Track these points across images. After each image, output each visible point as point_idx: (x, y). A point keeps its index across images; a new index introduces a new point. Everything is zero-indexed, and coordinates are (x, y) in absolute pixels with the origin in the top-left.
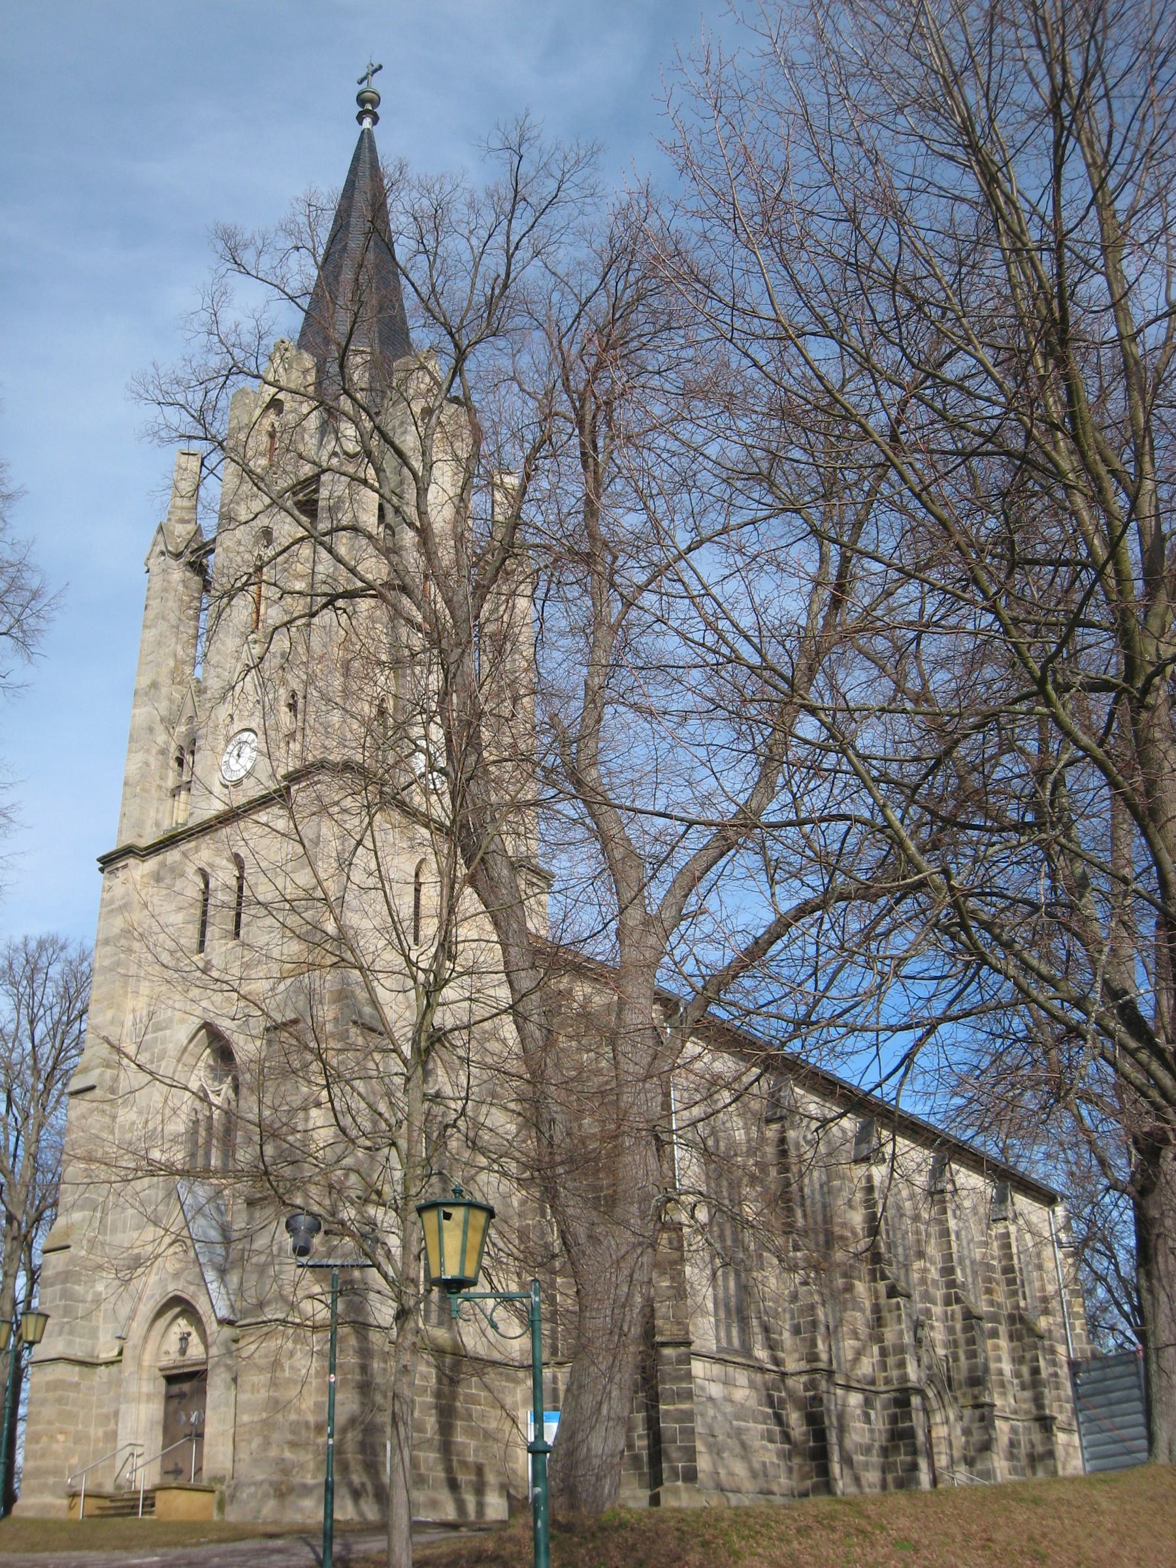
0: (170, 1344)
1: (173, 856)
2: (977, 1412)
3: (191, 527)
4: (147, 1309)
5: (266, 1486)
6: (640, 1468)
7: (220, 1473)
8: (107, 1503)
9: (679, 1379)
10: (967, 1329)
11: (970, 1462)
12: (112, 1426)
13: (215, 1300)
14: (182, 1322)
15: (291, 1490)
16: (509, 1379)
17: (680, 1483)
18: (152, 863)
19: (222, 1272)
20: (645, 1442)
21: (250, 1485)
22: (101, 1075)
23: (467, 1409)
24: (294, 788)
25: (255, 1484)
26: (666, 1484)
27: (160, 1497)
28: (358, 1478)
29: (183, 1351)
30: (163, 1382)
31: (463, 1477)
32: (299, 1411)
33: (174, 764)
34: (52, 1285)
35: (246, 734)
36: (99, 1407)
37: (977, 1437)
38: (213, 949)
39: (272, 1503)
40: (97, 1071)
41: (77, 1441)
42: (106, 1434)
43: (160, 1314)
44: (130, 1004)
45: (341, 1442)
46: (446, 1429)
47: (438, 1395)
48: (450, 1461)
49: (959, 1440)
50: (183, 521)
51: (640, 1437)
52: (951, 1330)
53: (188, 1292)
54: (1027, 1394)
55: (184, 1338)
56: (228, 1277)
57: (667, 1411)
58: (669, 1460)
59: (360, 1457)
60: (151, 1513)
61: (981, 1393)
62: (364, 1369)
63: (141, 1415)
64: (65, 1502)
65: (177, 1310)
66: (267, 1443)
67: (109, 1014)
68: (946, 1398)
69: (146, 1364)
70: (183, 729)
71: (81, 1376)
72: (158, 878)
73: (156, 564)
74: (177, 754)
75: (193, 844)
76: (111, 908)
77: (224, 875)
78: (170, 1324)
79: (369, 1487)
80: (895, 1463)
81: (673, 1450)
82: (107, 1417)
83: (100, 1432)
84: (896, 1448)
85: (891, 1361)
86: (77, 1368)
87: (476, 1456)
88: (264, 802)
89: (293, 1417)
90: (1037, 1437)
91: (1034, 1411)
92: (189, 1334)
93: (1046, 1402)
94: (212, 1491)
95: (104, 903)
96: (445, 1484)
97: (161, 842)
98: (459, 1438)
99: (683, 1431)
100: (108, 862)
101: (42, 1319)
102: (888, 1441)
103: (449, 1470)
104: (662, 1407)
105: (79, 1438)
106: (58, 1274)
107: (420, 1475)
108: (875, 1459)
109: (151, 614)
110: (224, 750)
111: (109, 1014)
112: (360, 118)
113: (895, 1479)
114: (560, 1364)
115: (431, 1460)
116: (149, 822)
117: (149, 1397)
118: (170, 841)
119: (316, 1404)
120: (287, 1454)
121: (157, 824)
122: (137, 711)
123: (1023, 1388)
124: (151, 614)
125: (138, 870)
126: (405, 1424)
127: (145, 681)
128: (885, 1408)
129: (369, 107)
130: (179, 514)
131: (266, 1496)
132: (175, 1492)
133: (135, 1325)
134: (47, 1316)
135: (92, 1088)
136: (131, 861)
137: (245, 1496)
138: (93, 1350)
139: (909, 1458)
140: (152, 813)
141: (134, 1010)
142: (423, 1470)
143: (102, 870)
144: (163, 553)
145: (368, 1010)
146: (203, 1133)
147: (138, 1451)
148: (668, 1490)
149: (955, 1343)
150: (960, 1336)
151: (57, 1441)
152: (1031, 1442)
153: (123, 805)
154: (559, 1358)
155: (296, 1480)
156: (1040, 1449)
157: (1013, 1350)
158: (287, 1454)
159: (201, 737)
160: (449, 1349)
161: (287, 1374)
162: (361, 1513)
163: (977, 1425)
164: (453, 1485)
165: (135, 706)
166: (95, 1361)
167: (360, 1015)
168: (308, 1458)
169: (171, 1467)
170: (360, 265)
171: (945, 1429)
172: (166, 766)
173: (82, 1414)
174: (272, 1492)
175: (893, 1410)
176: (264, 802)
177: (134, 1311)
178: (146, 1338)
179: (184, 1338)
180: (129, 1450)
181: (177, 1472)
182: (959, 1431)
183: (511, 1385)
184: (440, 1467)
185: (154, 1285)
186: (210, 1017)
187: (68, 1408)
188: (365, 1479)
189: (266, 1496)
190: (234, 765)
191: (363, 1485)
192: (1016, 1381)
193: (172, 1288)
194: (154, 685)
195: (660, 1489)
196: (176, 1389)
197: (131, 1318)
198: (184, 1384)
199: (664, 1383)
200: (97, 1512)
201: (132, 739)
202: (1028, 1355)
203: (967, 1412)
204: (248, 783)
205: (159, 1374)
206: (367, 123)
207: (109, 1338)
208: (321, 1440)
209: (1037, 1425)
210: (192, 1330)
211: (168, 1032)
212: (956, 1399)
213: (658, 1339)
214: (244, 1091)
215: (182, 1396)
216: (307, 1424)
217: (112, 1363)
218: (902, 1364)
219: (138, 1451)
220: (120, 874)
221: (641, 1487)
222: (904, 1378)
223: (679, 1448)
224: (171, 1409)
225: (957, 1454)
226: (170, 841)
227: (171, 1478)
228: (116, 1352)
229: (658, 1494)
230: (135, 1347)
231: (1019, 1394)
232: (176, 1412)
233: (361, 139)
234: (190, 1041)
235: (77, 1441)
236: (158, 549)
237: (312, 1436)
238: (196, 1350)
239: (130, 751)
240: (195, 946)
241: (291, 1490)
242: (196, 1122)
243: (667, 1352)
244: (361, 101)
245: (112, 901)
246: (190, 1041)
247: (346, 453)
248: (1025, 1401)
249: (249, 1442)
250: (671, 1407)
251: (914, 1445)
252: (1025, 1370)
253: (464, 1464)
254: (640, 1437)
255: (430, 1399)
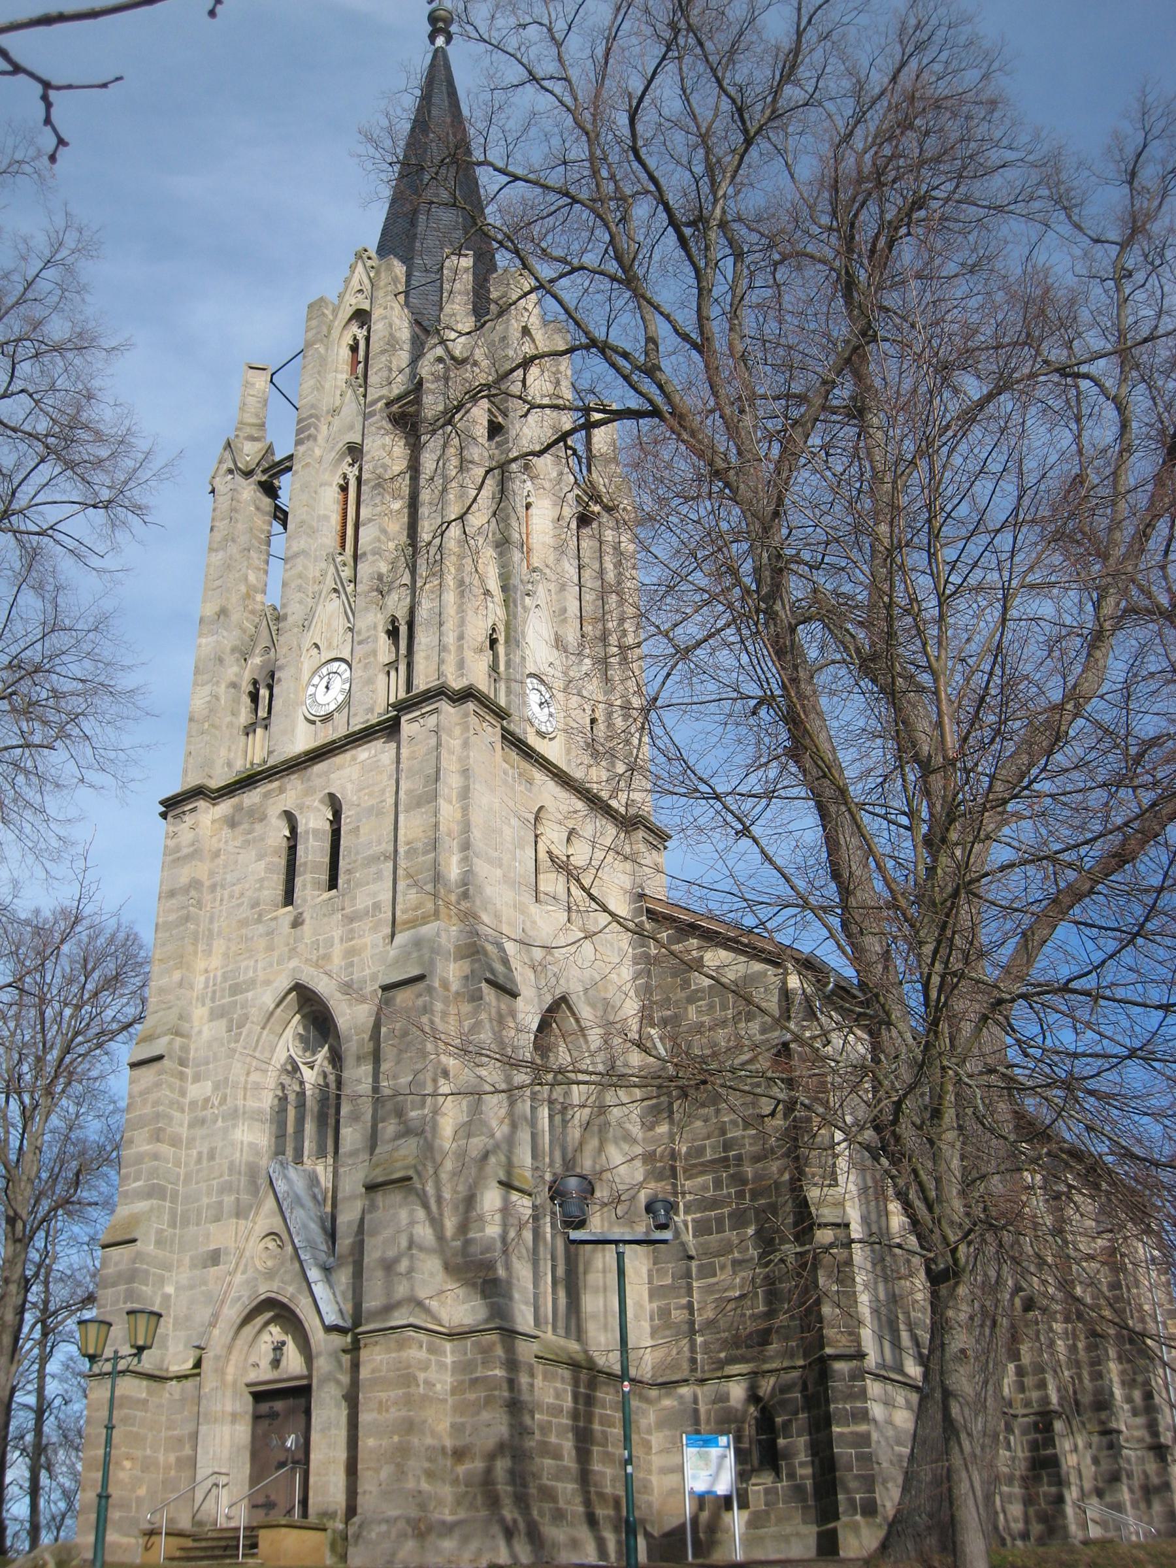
0: (261, 1356)
1: (251, 798)
2: (1105, 1440)
3: (258, 446)
4: (232, 1313)
5: (401, 1524)
6: (804, 1500)
7: (331, 1509)
8: (189, 1543)
9: (850, 1397)
10: (1090, 1348)
11: (1100, 1493)
12: (187, 1451)
13: (325, 1302)
14: (275, 1329)
15: (430, 1529)
16: (647, 1400)
17: (858, 1517)
18: (225, 807)
19: (327, 1270)
20: (808, 1471)
21: (379, 1523)
22: (171, 1042)
23: (603, 1432)
24: (403, 719)
25: (387, 1521)
26: (844, 1519)
27: (264, 1536)
28: (509, 1513)
29: (276, 1363)
30: (250, 1399)
31: (602, 1512)
32: (433, 1434)
33: (247, 700)
34: (114, 1285)
35: (336, 664)
36: (168, 1428)
37: (1105, 1465)
38: (305, 901)
39: (410, 1544)
40: (165, 1039)
41: (145, 1468)
42: (178, 1460)
43: (247, 1319)
44: (201, 964)
45: (489, 1471)
46: (583, 1455)
47: (575, 1415)
48: (588, 1492)
49: (1089, 1470)
50: (252, 439)
51: (802, 1464)
52: (1073, 1349)
53: (288, 1291)
54: (1140, 1420)
55: (279, 1348)
56: (334, 1277)
57: (841, 1434)
58: (847, 1491)
59: (509, 1488)
60: (253, 1555)
61: (1109, 1419)
62: (512, 1383)
63: (226, 1440)
64: (142, 1541)
65: (269, 1315)
66: (401, 1472)
67: (177, 976)
68: (1074, 1423)
69: (229, 1378)
70: (257, 660)
71: (150, 1393)
72: (232, 823)
73: (223, 484)
74: (251, 688)
75: (276, 784)
76: (175, 857)
77: (315, 821)
78: (260, 1332)
79: (522, 1525)
80: (1038, 1494)
81: (850, 1478)
82: (180, 1440)
83: (172, 1458)
84: (1037, 1479)
85: (1029, 1381)
86: (145, 1383)
87: (613, 1487)
88: (365, 735)
89: (429, 1441)
90: (1152, 1467)
91: (1148, 1439)
92: (283, 1343)
93: (1161, 1429)
94: (325, 1530)
95: (167, 851)
96: (583, 1519)
97: (236, 782)
98: (596, 1467)
99: (861, 1457)
100: (172, 805)
101: (154, 1319)
102: (1029, 1470)
103: (587, 1503)
104: (836, 1429)
105: (147, 1465)
106: (119, 1275)
107: (558, 1510)
108: (1017, 1490)
109: (218, 536)
110: (309, 683)
111: (177, 976)
112: (432, 38)
113: (1037, 1512)
114: (702, 1381)
115: (569, 1491)
116: (219, 762)
117: (234, 1417)
118: (248, 781)
119: (453, 1425)
120: (425, 1486)
121: (229, 765)
122: (204, 641)
123: (1135, 1414)
124: (218, 536)
125: (208, 815)
126: (970, 1435)
127: (210, 610)
128: (1024, 1433)
129: (441, 25)
130: (249, 431)
131: (403, 1535)
132: (284, 1530)
133: (216, 1332)
134: (110, 1325)
135: (160, 1058)
136: (202, 804)
137: (373, 1535)
138: (162, 1361)
139: (1053, 1490)
140: (223, 752)
141: (206, 971)
142: (561, 1504)
143: (164, 815)
144: (230, 471)
145: (499, 968)
146: (291, 1113)
147: (223, 1480)
148: (846, 1525)
149: (1078, 1364)
150: (1082, 1355)
151: (123, 1469)
152: (1145, 1472)
153: (189, 743)
154: (699, 1375)
155: (436, 1516)
156: (1156, 1480)
157: (1123, 1373)
158: (425, 1486)
159: (281, 668)
160: (584, 1363)
161: (421, 1390)
162: (513, 1555)
163: (1105, 1453)
164: (592, 1521)
165: (201, 635)
166: (164, 1374)
167: (492, 971)
168: (447, 1491)
169: (261, 1500)
170: (434, 182)
171: (1075, 1453)
172: (237, 701)
173: (150, 1435)
174: (410, 1531)
175: (1033, 1436)
176: (365, 735)
177: (216, 1316)
178: (230, 1348)
179: (279, 1348)
180: (209, 1483)
181: (269, 1505)
182: (1089, 1460)
183: (644, 1406)
184: (578, 1500)
185: (240, 1286)
186: (305, 979)
187: (135, 1429)
188: (517, 1516)
189: (403, 1535)
190: (321, 697)
191: (515, 1521)
192: (1126, 1407)
193: (265, 1290)
194: (223, 612)
195: (838, 1524)
196: (264, 1407)
197: (213, 1325)
198: (280, 1405)
199: (836, 1401)
200: (178, 1554)
201: (197, 671)
202: (1140, 1378)
203: (1095, 1439)
204: (340, 719)
205: (246, 1391)
206: (440, 41)
207: (181, 1347)
208: (461, 1470)
209: (1151, 1454)
210: (289, 1340)
211: (250, 995)
212: (1083, 1424)
213: (829, 1351)
214: (349, 1061)
215: (273, 1415)
216: (443, 1448)
217: (186, 1377)
218: (1042, 1385)
219: (223, 1480)
220: (186, 818)
221: (805, 1522)
222: (1045, 1400)
223: (857, 1477)
224: (260, 1432)
225: (1088, 1485)
226: (248, 781)
227: (261, 1512)
228: (190, 1364)
229: (833, 1533)
230: (217, 1358)
231: (1130, 1421)
232: (266, 1435)
233: (434, 57)
234: (278, 1005)
235: (145, 1468)
236: (225, 467)
237: (449, 1463)
238: (293, 1362)
239: (196, 684)
240: (280, 897)
241: (430, 1529)
242: (283, 1099)
243: (839, 1366)
244: (433, 19)
245: (178, 848)
246: (278, 1005)
247: (453, 358)
248: (1137, 1428)
249: (377, 1470)
250: (845, 1430)
251: (1058, 1475)
252: (1137, 1395)
253: (601, 1495)
254: (802, 1464)
255: (566, 1421)
